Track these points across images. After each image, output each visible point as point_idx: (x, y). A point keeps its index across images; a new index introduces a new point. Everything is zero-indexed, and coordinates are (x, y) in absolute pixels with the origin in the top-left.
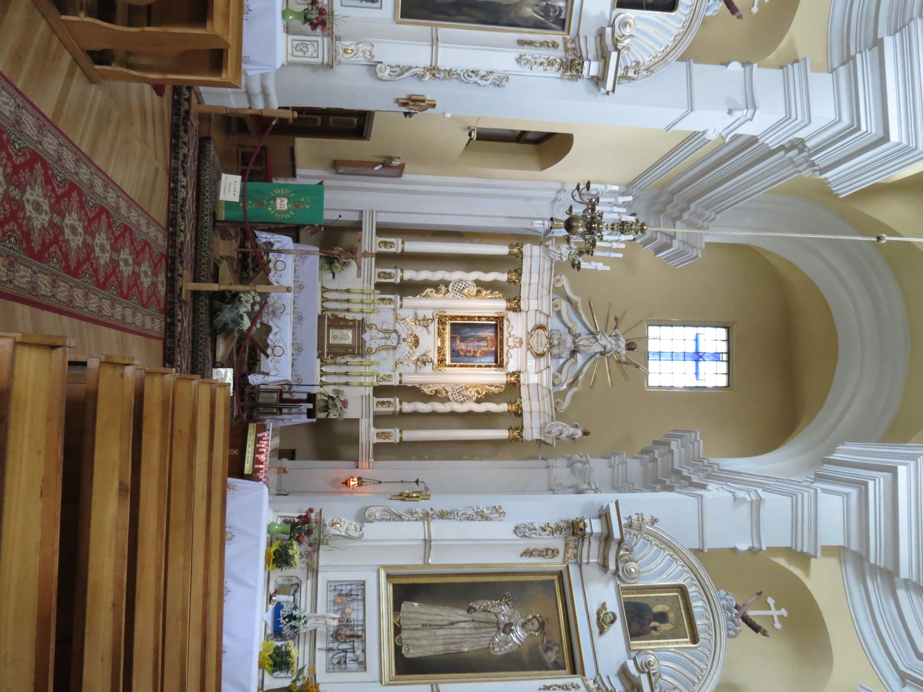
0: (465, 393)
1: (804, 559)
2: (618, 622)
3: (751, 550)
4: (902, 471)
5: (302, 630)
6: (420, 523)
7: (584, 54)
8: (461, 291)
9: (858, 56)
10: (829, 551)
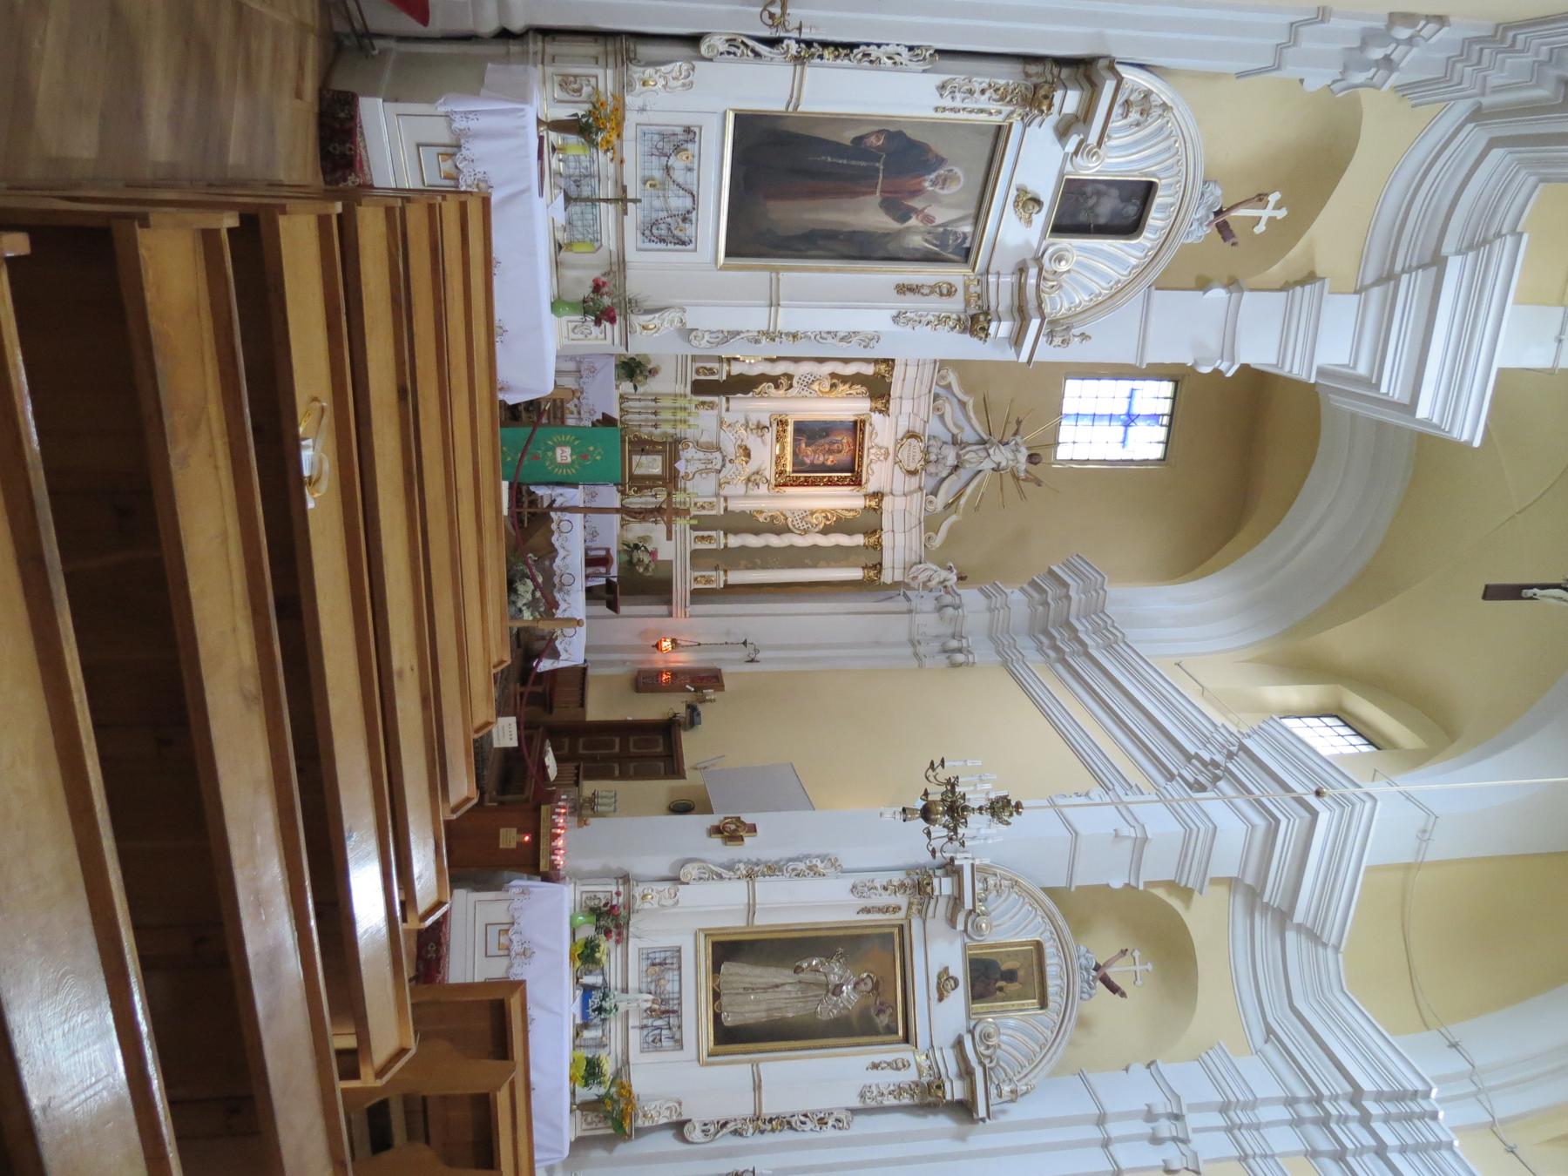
1: (1186, 894)
3: (1128, 885)
7: (993, 308)
9: (1405, 277)
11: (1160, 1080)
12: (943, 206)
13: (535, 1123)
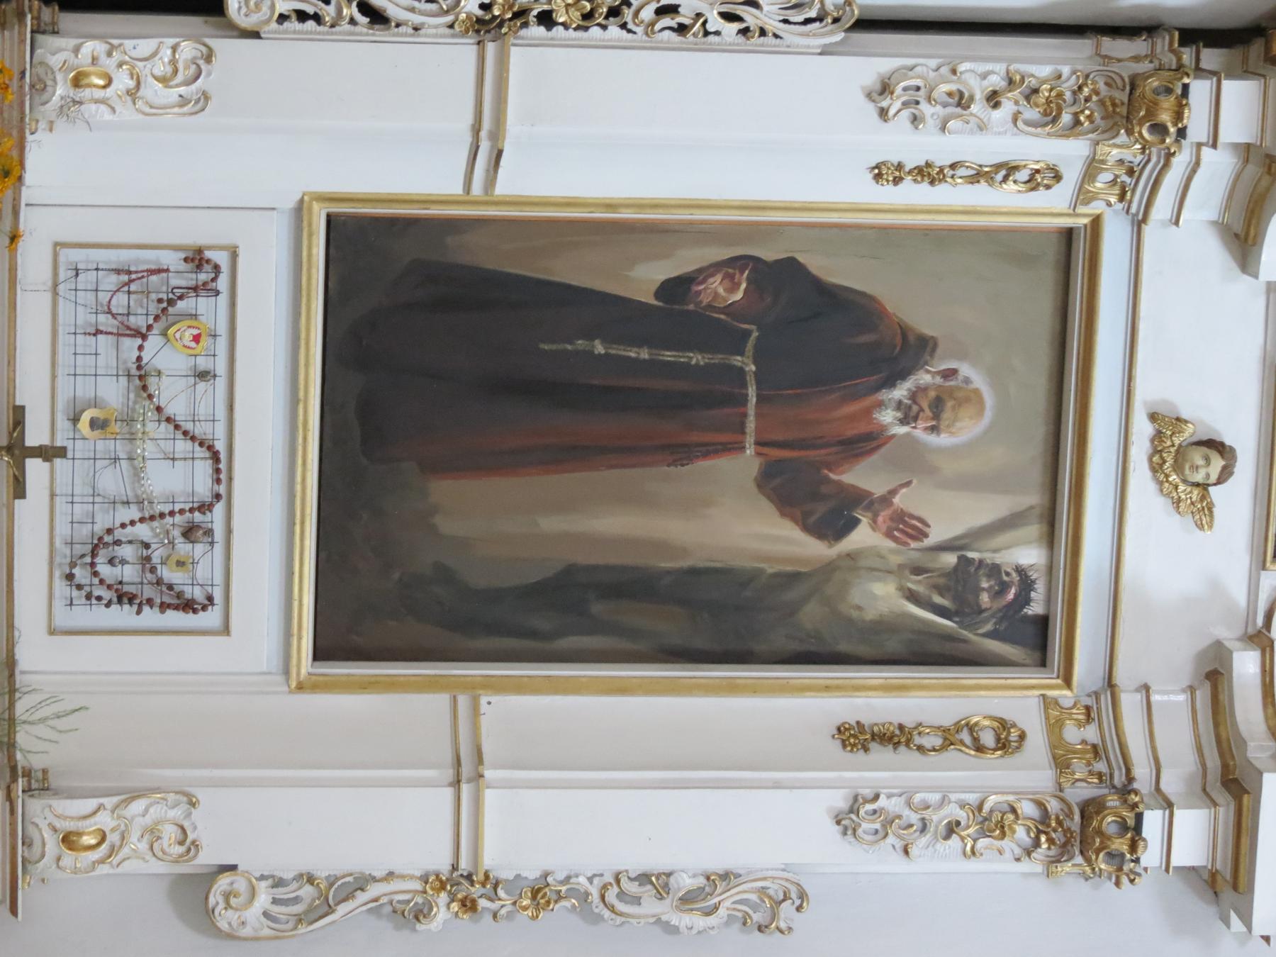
7: (1142, 772)
12: (944, 481)
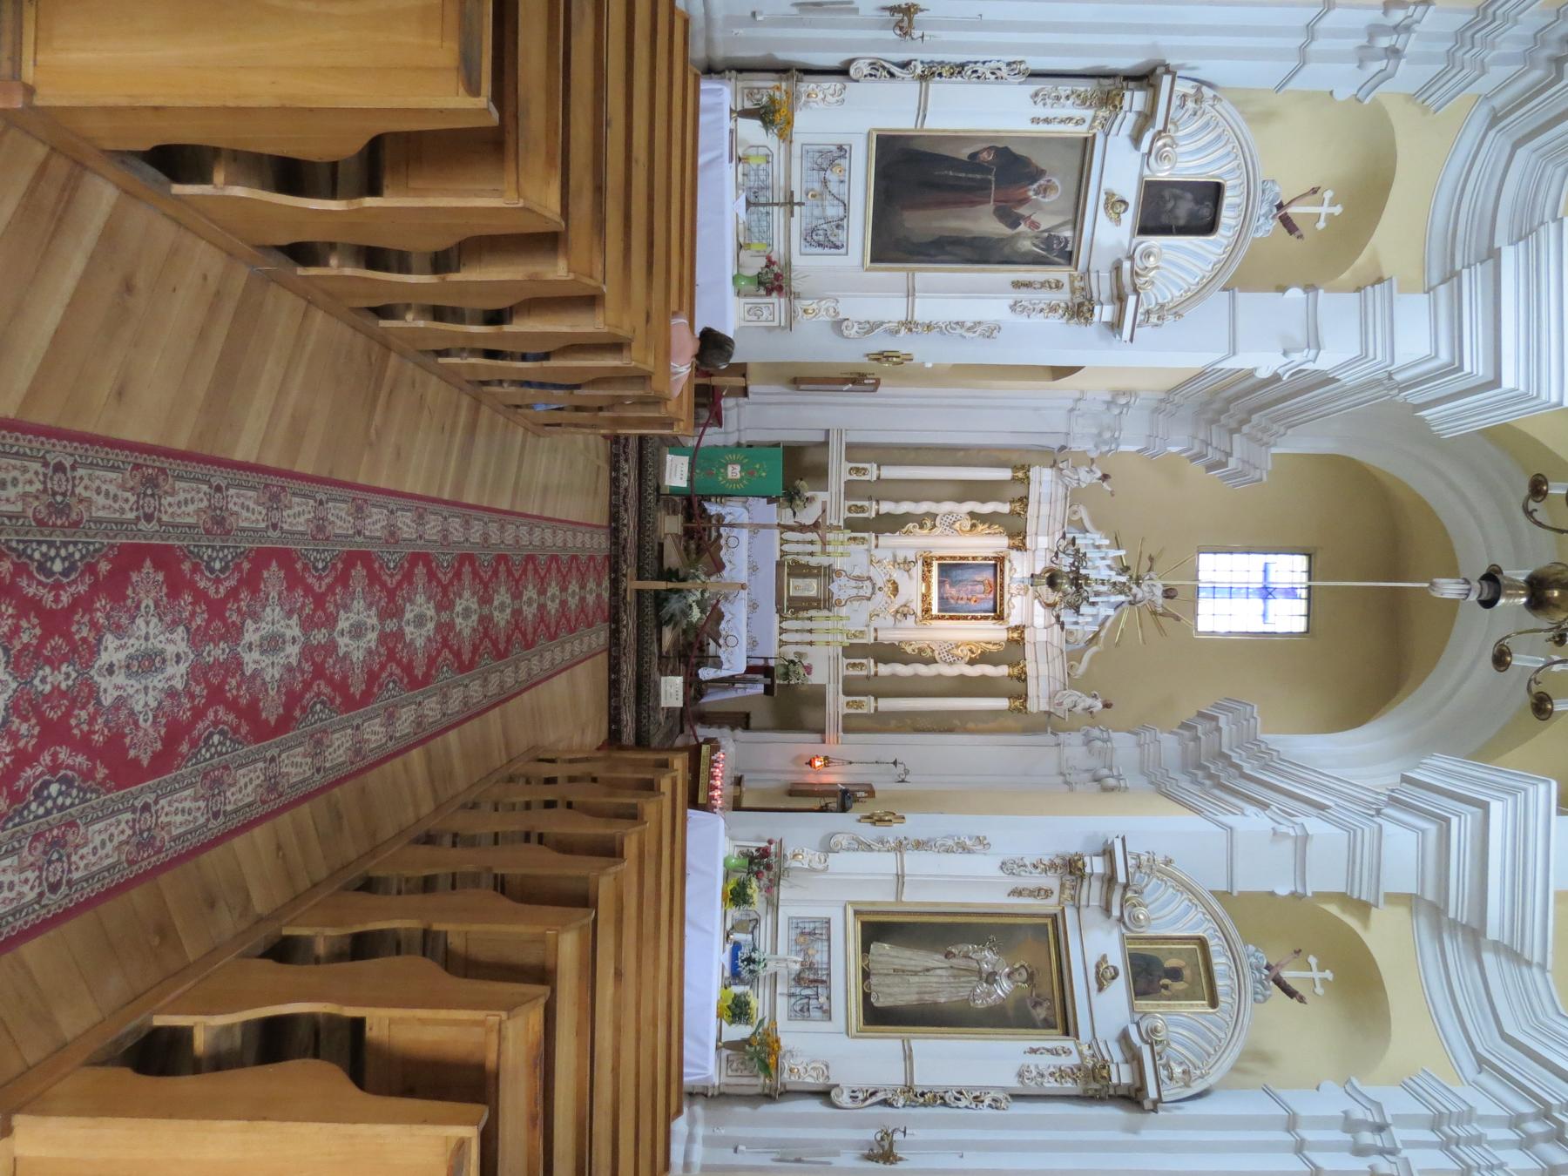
0: (955, 651)
1: (1362, 908)
2: (1121, 978)
3: (1293, 894)
4: (1496, 808)
5: (762, 973)
6: (892, 855)
7: (1095, 295)
8: (951, 526)
9: (1465, 272)
10: (1394, 899)
11: (1354, 1094)
12: (1045, 212)
13: (686, 1041)
